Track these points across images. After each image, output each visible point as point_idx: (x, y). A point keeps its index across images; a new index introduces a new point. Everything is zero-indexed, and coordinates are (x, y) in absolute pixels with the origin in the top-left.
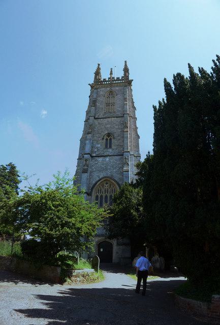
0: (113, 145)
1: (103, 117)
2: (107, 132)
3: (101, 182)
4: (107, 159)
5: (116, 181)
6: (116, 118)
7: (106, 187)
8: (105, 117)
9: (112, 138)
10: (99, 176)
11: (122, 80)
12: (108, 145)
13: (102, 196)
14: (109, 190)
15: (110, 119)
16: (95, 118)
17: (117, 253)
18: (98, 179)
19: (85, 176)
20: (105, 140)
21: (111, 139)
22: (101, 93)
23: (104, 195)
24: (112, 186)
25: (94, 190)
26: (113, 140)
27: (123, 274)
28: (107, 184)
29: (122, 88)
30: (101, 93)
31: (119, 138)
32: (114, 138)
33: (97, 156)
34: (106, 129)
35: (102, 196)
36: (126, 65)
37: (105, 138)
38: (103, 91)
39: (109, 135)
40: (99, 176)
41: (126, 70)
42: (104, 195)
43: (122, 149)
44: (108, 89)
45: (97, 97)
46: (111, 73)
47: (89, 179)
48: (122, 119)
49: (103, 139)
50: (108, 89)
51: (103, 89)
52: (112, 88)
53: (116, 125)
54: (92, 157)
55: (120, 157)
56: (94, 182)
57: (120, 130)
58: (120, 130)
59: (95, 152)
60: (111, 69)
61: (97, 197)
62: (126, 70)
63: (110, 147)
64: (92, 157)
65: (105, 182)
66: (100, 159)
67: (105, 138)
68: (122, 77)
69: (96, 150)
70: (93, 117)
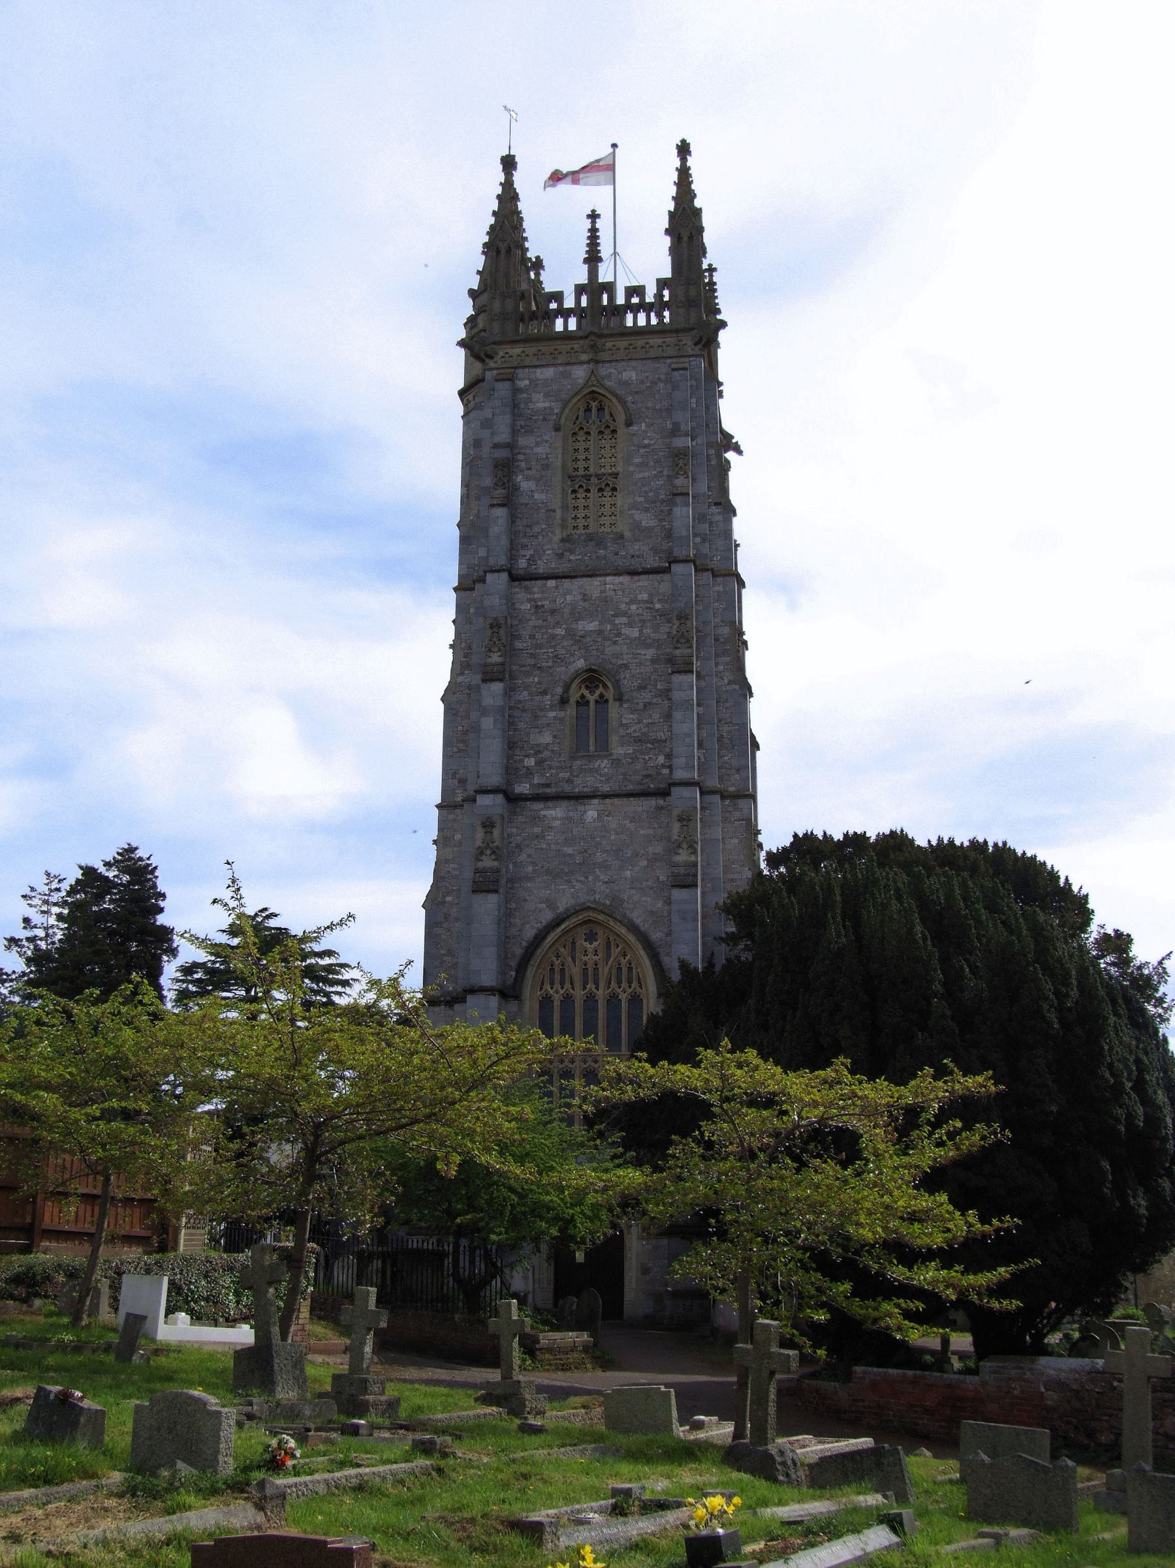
0: (614, 739)
1: (555, 566)
2: (581, 664)
3: (565, 932)
4: (592, 814)
5: (633, 928)
6: (625, 579)
7: (590, 953)
8: (564, 567)
9: (610, 695)
10: (551, 904)
11: (659, 306)
12: (589, 734)
13: (568, 1000)
14: (604, 972)
15: (596, 582)
16: (514, 578)
17: (645, 1270)
18: (547, 916)
19: (488, 905)
20: (571, 710)
21: (602, 701)
22: (540, 402)
23: (579, 994)
24: (615, 952)
25: (530, 973)
26: (614, 710)
27: (730, 473)
28: (591, 937)
29: (663, 367)
30: (540, 402)
31: (646, 696)
32: (619, 698)
33: (536, 798)
34: (578, 640)
35: (568, 1000)
36: (684, 174)
37: (574, 696)
38: (548, 385)
39: (591, 678)
40: (551, 904)
41: (685, 225)
42: (579, 994)
43: (661, 759)
44: (580, 373)
45: (514, 432)
46: (593, 258)
47: (506, 918)
48: (663, 585)
49: (564, 701)
50: (580, 373)
51: (549, 372)
52: (603, 370)
53: (630, 625)
54: (513, 799)
55: (652, 802)
56: (529, 933)
57: (650, 653)
58: (650, 653)
59: (529, 772)
60: (410, 962)
61: (546, 1002)
62: (685, 225)
63: (604, 746)
64: (513, 799)
65: (582, 931)
66: (555, 813)
67: (574, 696)
68: (662, 284)
69: (530, 762)
70: (504, 576)
